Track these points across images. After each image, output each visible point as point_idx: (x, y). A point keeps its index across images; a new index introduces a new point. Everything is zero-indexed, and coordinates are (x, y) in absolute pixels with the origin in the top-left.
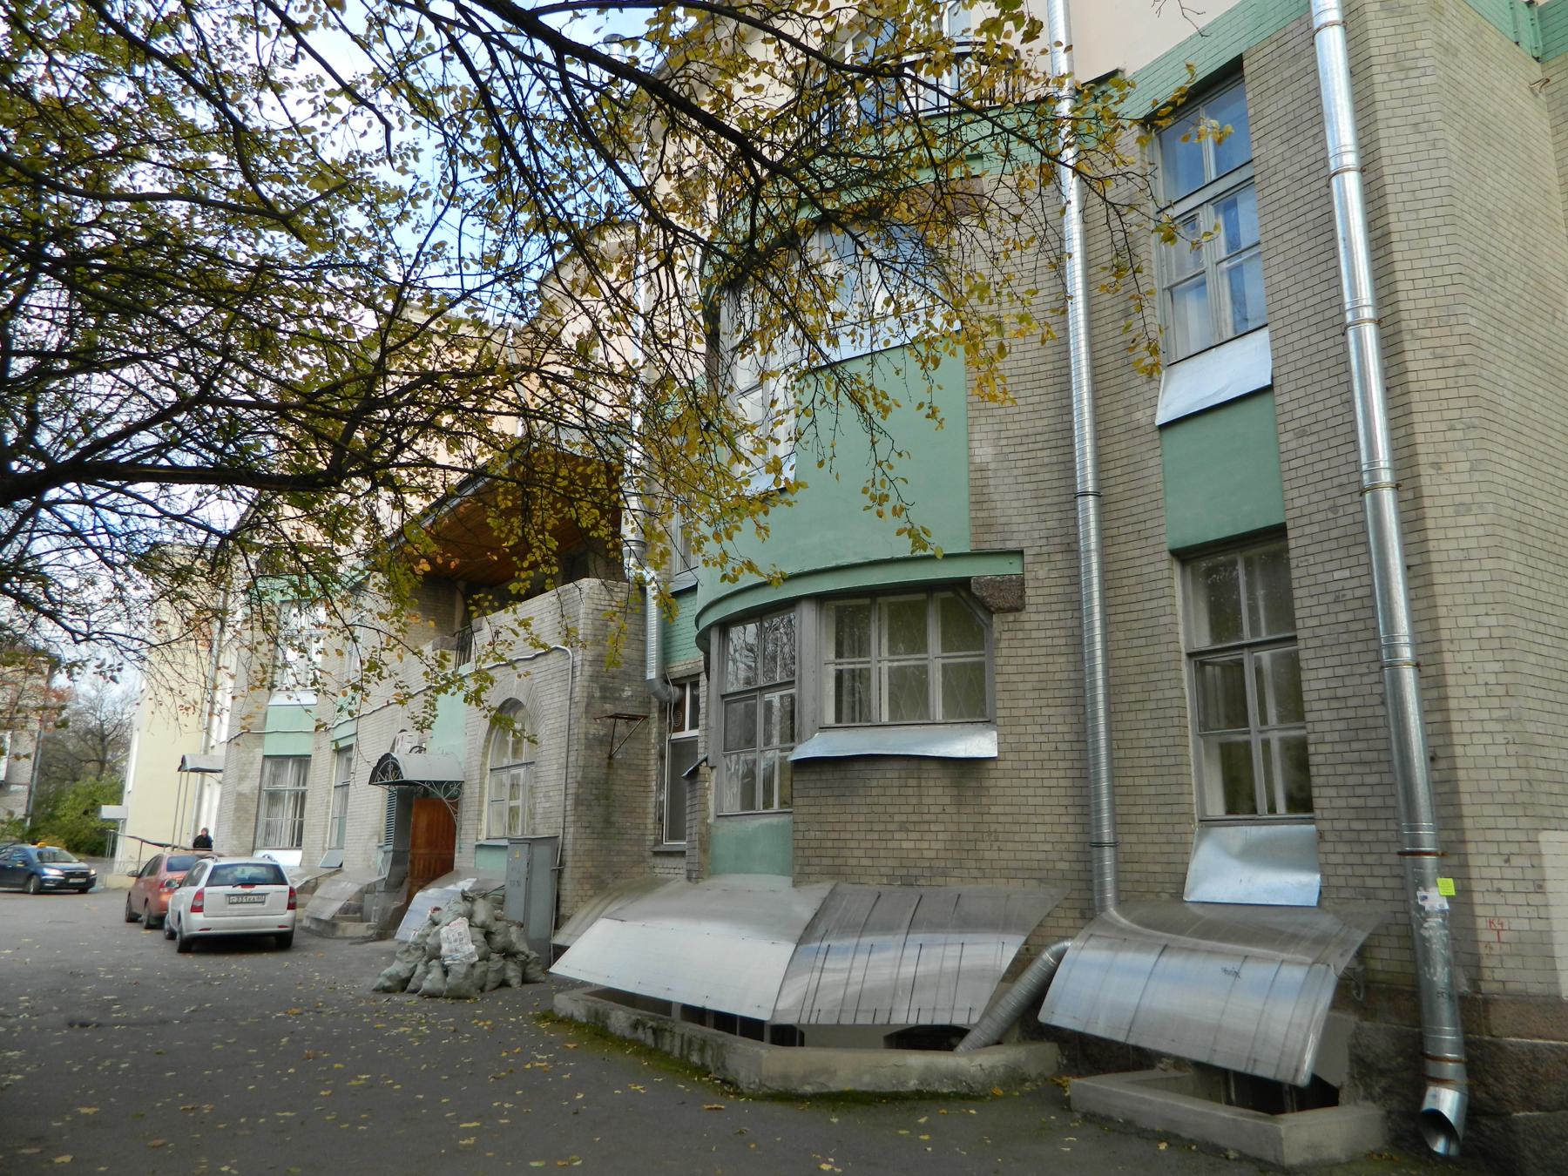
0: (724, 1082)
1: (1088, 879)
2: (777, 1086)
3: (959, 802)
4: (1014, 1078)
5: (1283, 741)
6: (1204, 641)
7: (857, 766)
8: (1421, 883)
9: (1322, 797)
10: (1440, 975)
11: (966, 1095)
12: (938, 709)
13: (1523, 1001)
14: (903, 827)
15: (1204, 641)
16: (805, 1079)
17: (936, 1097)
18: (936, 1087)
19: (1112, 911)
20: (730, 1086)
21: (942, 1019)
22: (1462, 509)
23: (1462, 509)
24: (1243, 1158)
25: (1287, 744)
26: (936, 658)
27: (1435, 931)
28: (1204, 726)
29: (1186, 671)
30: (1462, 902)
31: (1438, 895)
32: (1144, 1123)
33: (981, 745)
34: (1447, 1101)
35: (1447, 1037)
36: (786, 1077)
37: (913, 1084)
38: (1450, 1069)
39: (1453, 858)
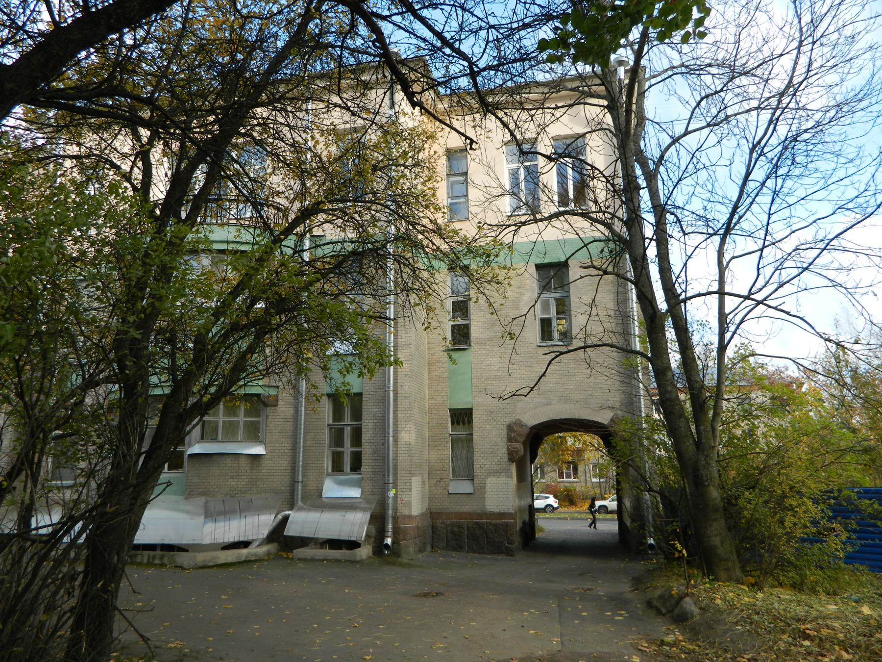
0: (176, 567)
1: (293, 492)
2: (201, 564)
3: (252, 469)
4: (269, 554)
5: (246, 422)
6: (331, 422)
7: (215, 457)
8: (388, 490)
9: (364, 468)
10: (390, 512)
11: (259, 560)
12: (240, 438)
13: (405, 517)
14: (232, 477)
15: (331, 422)
16: (210, 561)
17: (250, 561)
18: (250, 558)
19: (300, 502)
20: (182, 568)
21: (242, 539)
22: (406, 398)
23: (406, 398)
24: (346, 561)
25: (353, 453)
26: (241, 418)
27: (390, 501)
28: (330, 446)
29: (326, 430)
30: (396, 495)
31: (392, 493)
32: (317, 558)
33: (259, 450)
34: (389, 541)
35: (390, 527)
36: (204, 561)
37: (243, 559)
38: (390, 534)
39: (395, 487)
